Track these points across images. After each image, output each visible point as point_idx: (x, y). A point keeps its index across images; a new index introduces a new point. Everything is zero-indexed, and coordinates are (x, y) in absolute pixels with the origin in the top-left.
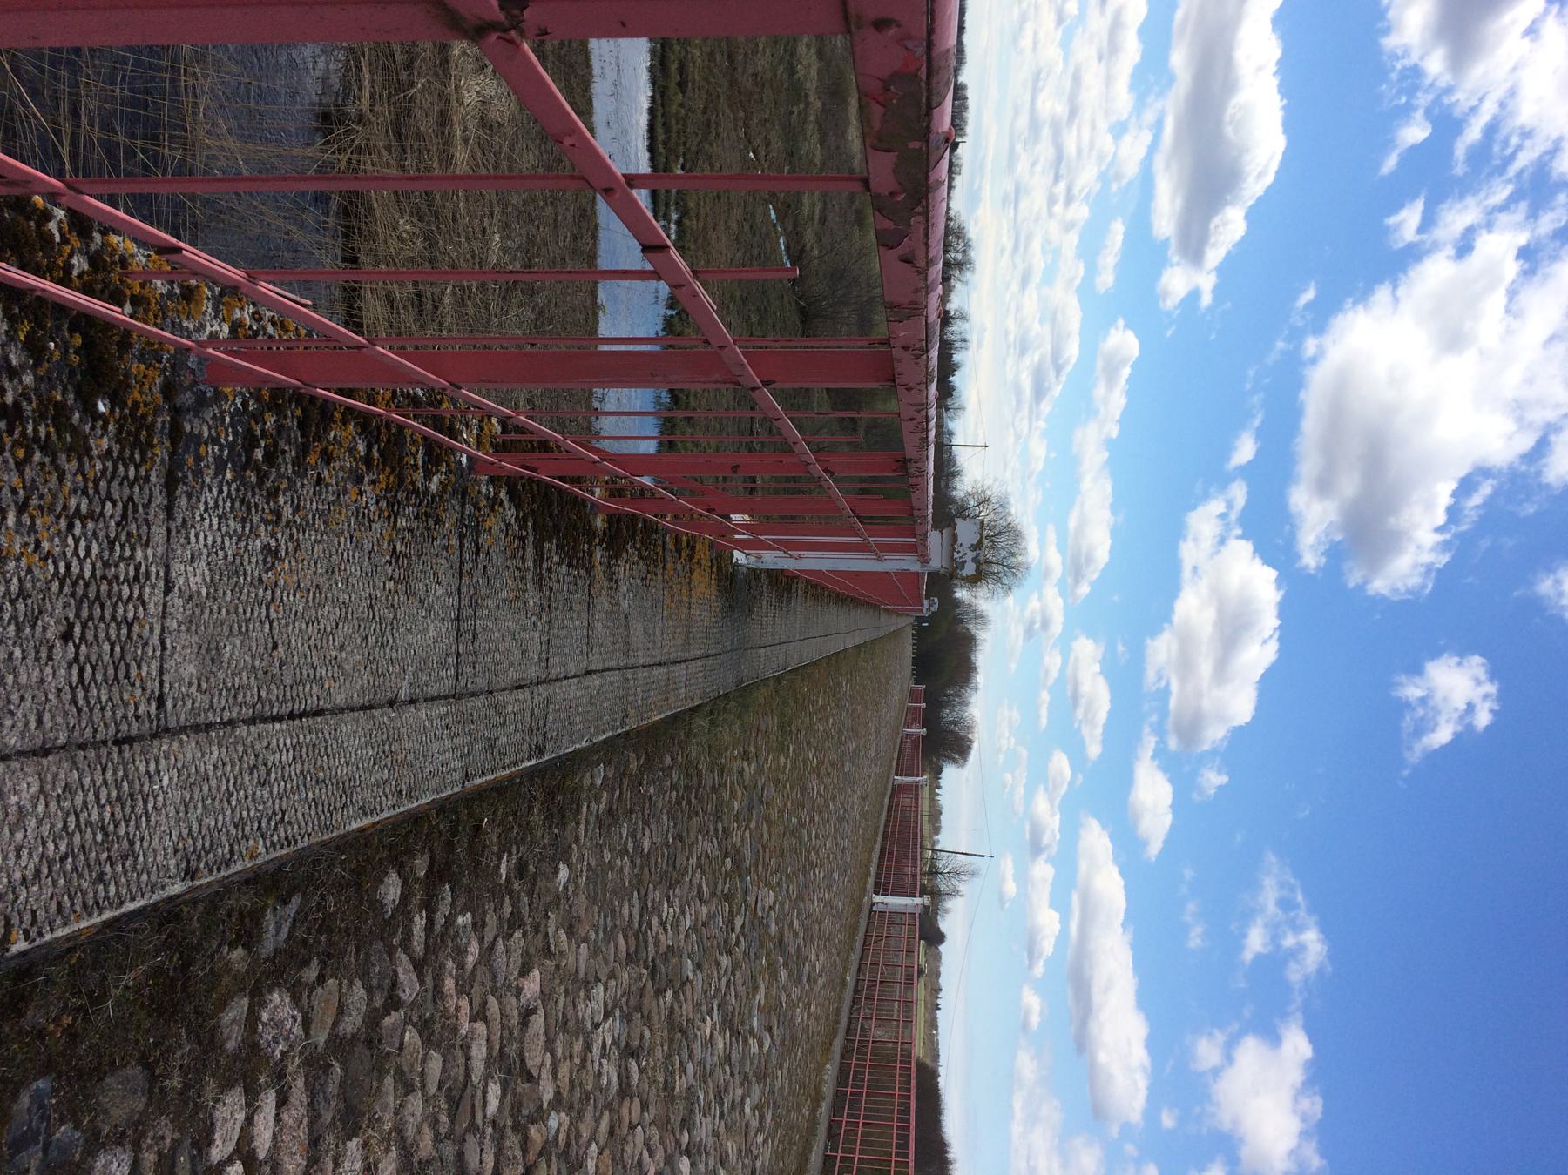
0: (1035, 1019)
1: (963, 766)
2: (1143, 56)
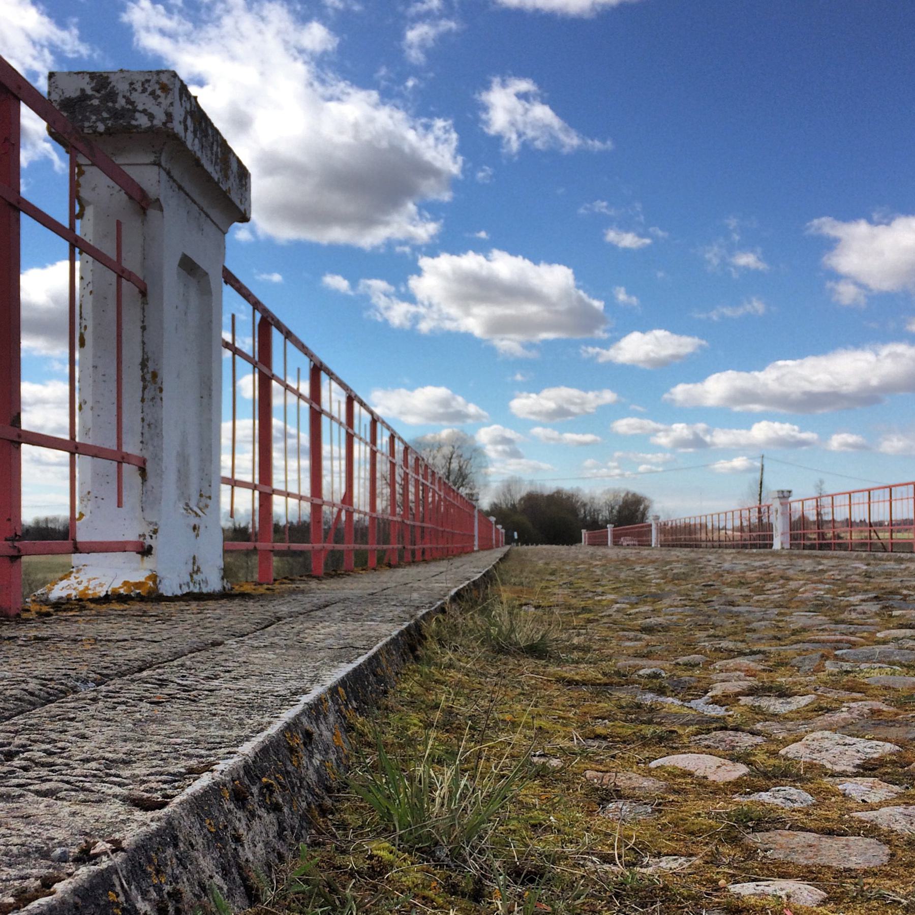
0: (851, 439)
1: (651, 502)
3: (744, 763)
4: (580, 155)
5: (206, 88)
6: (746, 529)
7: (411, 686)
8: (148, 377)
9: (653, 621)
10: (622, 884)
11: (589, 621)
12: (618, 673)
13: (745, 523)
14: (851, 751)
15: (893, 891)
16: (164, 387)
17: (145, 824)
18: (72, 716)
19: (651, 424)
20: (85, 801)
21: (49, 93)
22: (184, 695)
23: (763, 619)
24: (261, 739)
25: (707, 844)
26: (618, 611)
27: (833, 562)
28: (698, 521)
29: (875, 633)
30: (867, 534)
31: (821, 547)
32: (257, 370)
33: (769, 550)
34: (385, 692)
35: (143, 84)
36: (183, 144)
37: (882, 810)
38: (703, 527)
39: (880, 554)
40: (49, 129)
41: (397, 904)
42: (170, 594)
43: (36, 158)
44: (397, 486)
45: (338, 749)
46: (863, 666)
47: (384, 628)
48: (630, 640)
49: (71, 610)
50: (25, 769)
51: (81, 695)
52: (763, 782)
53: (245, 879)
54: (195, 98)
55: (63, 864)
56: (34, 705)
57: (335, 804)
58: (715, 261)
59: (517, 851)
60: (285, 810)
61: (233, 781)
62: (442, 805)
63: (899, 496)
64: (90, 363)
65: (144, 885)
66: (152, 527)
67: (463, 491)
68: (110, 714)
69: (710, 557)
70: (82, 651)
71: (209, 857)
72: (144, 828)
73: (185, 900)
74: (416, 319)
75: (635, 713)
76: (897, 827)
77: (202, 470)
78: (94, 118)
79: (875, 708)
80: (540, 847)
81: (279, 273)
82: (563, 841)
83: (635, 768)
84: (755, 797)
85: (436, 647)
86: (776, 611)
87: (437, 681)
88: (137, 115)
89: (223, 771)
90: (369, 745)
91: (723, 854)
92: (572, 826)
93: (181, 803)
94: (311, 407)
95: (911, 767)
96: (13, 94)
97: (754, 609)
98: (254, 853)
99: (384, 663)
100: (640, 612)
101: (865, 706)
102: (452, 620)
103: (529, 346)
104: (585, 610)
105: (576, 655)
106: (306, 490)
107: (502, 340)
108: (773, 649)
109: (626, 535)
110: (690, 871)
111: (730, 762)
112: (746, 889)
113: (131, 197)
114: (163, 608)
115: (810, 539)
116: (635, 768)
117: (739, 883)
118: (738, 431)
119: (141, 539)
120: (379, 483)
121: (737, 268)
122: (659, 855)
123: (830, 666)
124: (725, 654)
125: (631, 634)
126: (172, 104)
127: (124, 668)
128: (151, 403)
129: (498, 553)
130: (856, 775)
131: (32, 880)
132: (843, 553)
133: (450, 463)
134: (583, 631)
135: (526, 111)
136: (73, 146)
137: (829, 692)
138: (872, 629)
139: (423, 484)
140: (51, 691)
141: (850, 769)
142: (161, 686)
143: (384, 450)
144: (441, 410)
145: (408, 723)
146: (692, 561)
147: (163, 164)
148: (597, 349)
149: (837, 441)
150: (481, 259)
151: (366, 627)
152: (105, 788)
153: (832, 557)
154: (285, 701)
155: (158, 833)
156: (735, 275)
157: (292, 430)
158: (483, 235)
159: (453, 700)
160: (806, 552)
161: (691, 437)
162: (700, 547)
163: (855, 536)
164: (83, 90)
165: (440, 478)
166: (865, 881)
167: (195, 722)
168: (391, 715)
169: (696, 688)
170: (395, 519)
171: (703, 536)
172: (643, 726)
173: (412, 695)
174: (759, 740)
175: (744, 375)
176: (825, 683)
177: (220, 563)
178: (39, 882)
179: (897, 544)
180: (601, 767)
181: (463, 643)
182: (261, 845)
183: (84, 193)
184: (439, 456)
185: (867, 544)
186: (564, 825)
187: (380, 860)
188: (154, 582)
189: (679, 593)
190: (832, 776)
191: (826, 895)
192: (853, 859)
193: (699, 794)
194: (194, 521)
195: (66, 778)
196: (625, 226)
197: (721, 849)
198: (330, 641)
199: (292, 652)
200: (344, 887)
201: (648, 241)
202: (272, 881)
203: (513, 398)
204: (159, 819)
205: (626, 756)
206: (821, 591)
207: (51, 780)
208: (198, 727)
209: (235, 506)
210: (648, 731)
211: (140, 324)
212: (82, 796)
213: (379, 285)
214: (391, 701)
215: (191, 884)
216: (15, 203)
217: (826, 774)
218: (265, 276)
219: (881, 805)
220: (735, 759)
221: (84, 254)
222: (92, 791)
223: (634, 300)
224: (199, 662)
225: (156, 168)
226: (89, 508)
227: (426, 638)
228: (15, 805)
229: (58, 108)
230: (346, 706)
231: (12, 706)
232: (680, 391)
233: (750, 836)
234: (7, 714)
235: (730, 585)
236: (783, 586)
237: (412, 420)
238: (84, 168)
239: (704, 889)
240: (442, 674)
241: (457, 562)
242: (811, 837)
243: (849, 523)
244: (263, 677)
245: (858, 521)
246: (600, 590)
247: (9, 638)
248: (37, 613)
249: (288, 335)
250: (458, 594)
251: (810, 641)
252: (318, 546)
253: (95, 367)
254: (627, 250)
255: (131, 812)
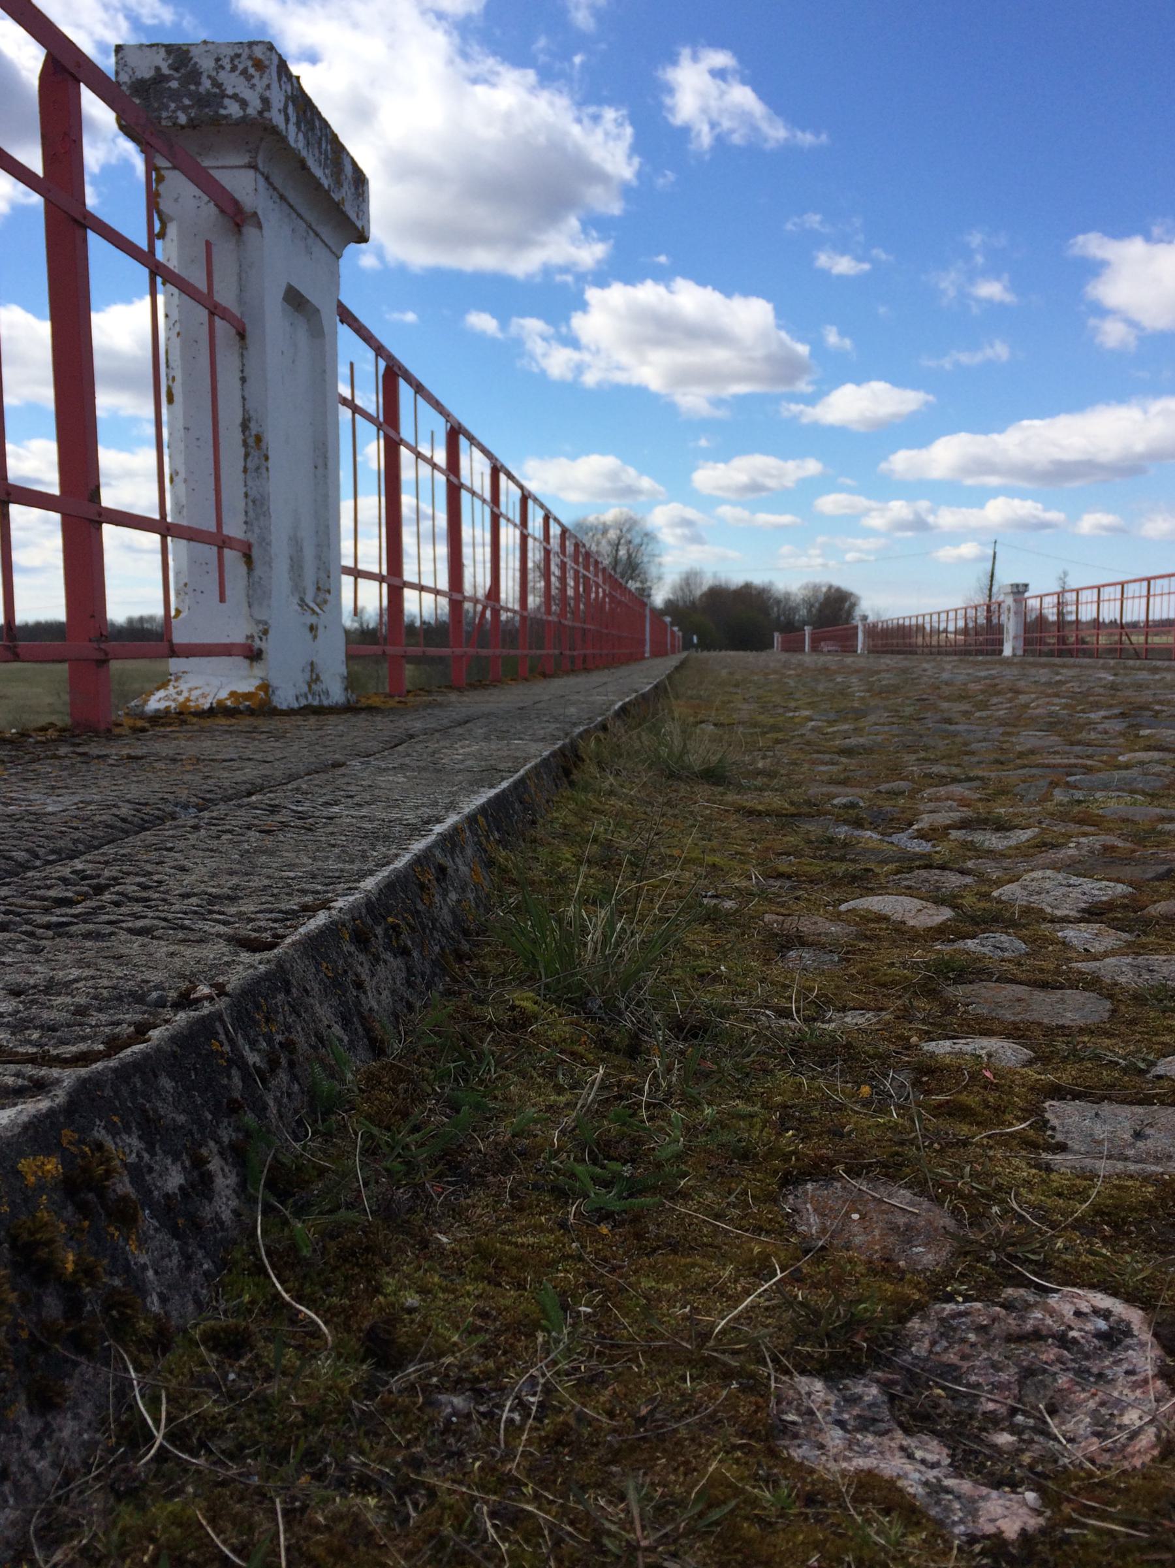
0: (1107, 519)
1: (858, 598)
2: (960, 431)
3: (950, 906)
4: (788, 151)
5: (320, 67)
6: (972, 632)
7: (564, 815)
8: (251, 441)
9: (853, 741)
10: (799, 1041)
11: (778, 741)
12: (808, 803)
13: (971, 625)
14: (1075, 893)
15: (1111, 1051)
16: (270, 454)
17: (252, 966)
18: (171, 845)
19: (862, 502)
20: (185, 941)
21: (117, 73)
22: (299, 823)
23: (984, 740)
24: (386, 874)
25: (900, 997)
26: (813, 729)
27: (1071, 672)
28: (914, 621)
29: (1116, 756)
30: (1117, 638)
31: (1061, 654)
32: (381, 433)
33: (996, 658)
34: (534, 822)
35: (232, 60)
36: (283, 139)
37: (1107, 960)
38: (920, 629)
39: (1131, 663)
40: (119, 120)
41: (540, 1060)
42: (284, 707)
43: (113, 161)
44: (553, 579)
45: (477, 887)
46: (1098, 795)
47: (534, 748)
48: (826, 764)
49: (170, 725)
50: (117, 904)
51: (180, 822)
52: (969, 928)
53: (368, 1031)
54: (298, 78)
55: (160, 1010)
56: (127, 833)
57: (474, 949)
58: (952, 293)
59: (681, 1004)
60: (415, 954)
61: (354, 920)
62: (595, 952)
63: (1158, 591)
64: (180, 425)
65: (252, 1033)
66: (261, 627)
67: (633, 585)
68: (214, 844)
69: (925, 666)
70: (183, 772)
71: (326, 1005)
72: (251, 971)
73: (301, 1052)
74: (580, 369)
75: (826, 848)
76: (1122, 980)
77: (318, 557)
78: (173, 106)
79: (1108, 843)
80: (706, 999)
81: (414, 312)
82: (735, 994)
83: (822, 912)
84: (960, 945)
85: (594, 770)
86: (1001, 730)
87: (595, 811)
88: (227, 101)
89: (341, 909)
90: (513, 882)
91: (918, 1009)
92: (745, 975)
93: (293, 944)
94: (448, 480)
95: (1145, 912)
96: (72, 74)
97: (974, 728)
98: (379, 1002)
99: (533, 789)
100: (838, 731)
101: (1093, 841)
102: (615, 739)
103: (718, 403)
104: (774, 728)
105: (759, 782)
106: (443, 584)
107: (685, 394)
108: (993, 775)
109: (829, 639)
110: (877, 1027)
111: (933, 906)
112: (942, 1048)
113: (222, 211)
114: (275, 724)
115: (1049, 644)
116: (822, 912)
117: (933, 1040)
118: (970, 511)
119: (249, 641)
120: (530, 576)
121: (978, 300)
122: (844, 1009)
123: (1059, 795)
124: (937, 781)
125: (827, 757)
126: (268, 87)
127: (230, 792)
128: (254, 474)
129: (673, 661)
130: (1080, 921)
131: (125, 1026)
132: (1088, 660)
133: (617, 550)
134: (771, 754)
135: (722, 94)
136: (148, 143)
137: (1055, 825)
138: (1113, 751)
139: (584, 576)
140: (146, 817)
141: (1073, 913)
142: (272, 812)
143: (537, 535)
144: (608, 485)
145: (559, 858)
146: (904, 671)
147: (260, 166)
148: (802, 407)
149: (1090, 522)
150: (661, 290)
151: (513, 747)
152: (207, 927)
153: (1074, 666)
154: (417, 831)
155: (267, 976)
156: (975, 310)
157: (426, 508)
158: (662, 259)
159: (613, 832)
160: (1043, 660)
161: (911, 517)
162: (916, 654)
163: (1103, 640)
164: (158, 69)
165: (604, 569)
166: (1079, 1039)
167: (311, 854)
168: (540, 849)
169: (899, 819)
170: (550, 618)
171: (920, 640)
172: (834, 864)
173: (565, 826)
174: (969, 880)
175: (981, 438)
176: (1053, 814)
177: (343, 670)
178: (132, 1029)
179: (1153, 649)
180: (782, 910)
181: (627, 766)
182: (386, 993)
183: (165, 205)
184: (604, 542)
185: (1116, 650)
186: (737, 975)
187: (523, 1011)
188: (266, 692)
189: (886, 709)
190: (1052, 921)
191: (1032, 1054)
192: (1069, 1014)
193: (894, 941)
194: (313, 620)
195: (162, 915)
196: (842, 247)
197: (915, 1003)
198: (468, 763)
199: (425, 775)
200: (482, 1041)
201: (866, 267)
202: (399, 1032)
203: (695, 468)
204: (269, 961)
205: (813, 898)
206: (1057, 706)
207: (145, 917)
208: (314, 859)
209: (360, 604)
210: (840, 869)
211: (239, 375)
212: (180, 935)
213: (534, 325)
214: (540, 832)
215: (307, 1036)
216: (80, 219)
217: (1044, 919)
218: (396, 316)
219: (1106, 954)
220: (939, 901)
221: (168, 285)
222: (193, 930)
223: (847, 343)
224: (317, 785)
225: (251, 173)
226: (187, 602)
227: (583, 760)
228: (105, 944)
229: (128, 93)
230: (487, 837)
231: (102, 834)
232: (902, 461)
233: (950, 989)
234: (96, 843)
235: (947, 699)
236: (1010, 700)
237: (573, 497)
238: (163, 172)
239: (892, 1047)
240: (601, 802)
241: (623, 671)
242: (1021, 990)
243: (1097, 624)
244: (391, 804)
245: (1107, 621)
246: (793, 704)
247: (99, 757)
248: (131, 728)
249: (419, 389)
250: (623, 709)
251: (1037, 766)
252: (458, 651)
253: (187, 429)
254: (841, 278)
255: (237, 954)
